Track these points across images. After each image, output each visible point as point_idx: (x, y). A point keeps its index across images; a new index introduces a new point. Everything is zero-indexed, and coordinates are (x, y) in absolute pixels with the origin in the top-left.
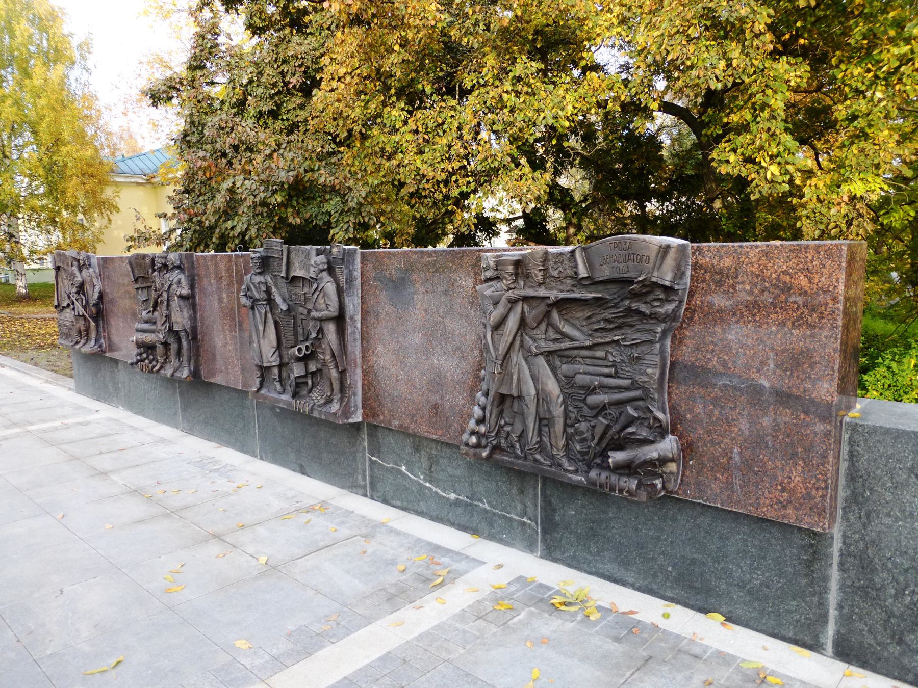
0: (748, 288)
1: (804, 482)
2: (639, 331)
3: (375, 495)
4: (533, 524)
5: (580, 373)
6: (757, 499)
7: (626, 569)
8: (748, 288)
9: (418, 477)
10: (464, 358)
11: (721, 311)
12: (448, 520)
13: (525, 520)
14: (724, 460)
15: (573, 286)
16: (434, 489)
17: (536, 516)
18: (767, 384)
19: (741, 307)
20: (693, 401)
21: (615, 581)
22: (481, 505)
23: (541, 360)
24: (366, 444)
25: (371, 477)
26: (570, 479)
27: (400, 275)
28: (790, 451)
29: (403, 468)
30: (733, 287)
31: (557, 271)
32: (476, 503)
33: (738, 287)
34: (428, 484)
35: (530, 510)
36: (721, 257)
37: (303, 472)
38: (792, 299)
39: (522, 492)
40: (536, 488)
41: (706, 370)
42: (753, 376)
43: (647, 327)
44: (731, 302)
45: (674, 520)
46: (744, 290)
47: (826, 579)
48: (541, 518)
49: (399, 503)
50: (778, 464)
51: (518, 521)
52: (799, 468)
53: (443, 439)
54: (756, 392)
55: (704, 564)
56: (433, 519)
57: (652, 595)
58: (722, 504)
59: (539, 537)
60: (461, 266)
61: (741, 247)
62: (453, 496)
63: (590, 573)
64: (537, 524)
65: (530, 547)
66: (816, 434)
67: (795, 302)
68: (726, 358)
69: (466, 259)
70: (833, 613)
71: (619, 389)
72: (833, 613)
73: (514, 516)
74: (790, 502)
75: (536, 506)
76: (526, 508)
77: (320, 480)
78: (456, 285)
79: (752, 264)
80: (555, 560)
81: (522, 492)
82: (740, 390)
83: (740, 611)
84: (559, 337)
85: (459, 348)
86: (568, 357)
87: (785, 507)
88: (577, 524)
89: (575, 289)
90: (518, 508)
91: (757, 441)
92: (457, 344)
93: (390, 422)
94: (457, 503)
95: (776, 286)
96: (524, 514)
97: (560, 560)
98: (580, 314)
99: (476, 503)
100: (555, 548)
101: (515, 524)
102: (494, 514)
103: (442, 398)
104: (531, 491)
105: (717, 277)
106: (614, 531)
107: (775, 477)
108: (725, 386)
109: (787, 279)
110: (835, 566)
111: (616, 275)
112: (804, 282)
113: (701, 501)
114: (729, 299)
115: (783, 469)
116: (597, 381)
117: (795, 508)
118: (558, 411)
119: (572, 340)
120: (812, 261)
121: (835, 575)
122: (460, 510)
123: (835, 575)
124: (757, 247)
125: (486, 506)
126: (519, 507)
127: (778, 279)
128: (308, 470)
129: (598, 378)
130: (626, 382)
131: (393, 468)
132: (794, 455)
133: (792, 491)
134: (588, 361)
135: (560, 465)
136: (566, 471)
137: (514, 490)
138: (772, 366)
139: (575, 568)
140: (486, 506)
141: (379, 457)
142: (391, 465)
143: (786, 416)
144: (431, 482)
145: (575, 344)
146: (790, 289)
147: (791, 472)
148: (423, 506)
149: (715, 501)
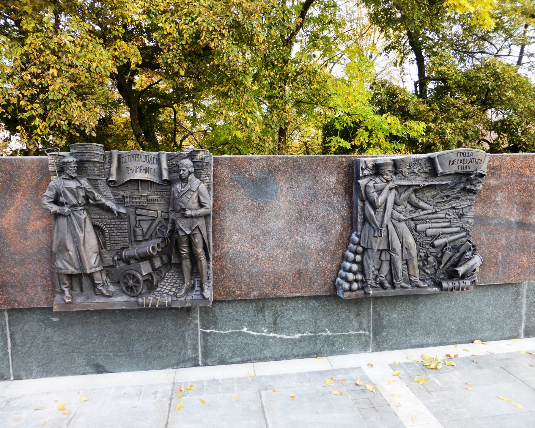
0: (506, 175)
1: (527, 261)
2: (463, 200)
3: (209, 361)
4: (367, 333)
5: (430, 228)
6: (509, 275)
7: (429, 337)
8: (506, 175)
9: (263, 332)
10: (327, 232)
11: (494, 187)
12: (292, 355)
13: (361, 332)
14: (494, 260)
15: (426, 178)
16: (278, 336)
17: (369, 327)
18: (513, 220)
19: (502, 184)
20: (481, 234)
21: (422, 346)
22: (324, 334)
23: (403, 224)
24: (198, 322)
25: (204, 347)
26: (428, 291)
27: (261, 176)
28: (522, 249)
29: (245, 330)
30: (499, 175)
31: (417, 169)
32: (320, 334)
33: (502, 175)
34: (272, 335)
35: (364, 325)
36: (494, 161)
37: (99, 369)
38: (523, 179)
39: (359, 314)
40: (369, 309)
41: (486, 217)
42: (508, 217)
43: (468, 198)
44: (498, 183)
45: (456, 300)
46: (504, 176)
47: (521, 304)
48: (373, 327)
49: (239, 359)
50: (517, 256)
51: (355, 335)
52: (526, 256)
53: (309, 294)
54: (509, 224)
55: (470, 318)
56: (276, 359)
57: (443, 345)
58: (493, 282)
59: (371, 339)
60: (326, 168)
61: (503, 156)
62: (297, 336)
63: (407, 348)
64: (369, 332)
65: (365, 347)
66: (532, 239)
67: (524, 181)
68: (496, 210)
69: (329, 163)
70: (524, 318)
71: (452, 233)
72: (524, 318)
73: (352, 333)
74: (522, 272)
75: (369, 320)
76: (356, 325)
77: (129, 370)
78: (320, 181)
79: (507, 164)
80: (383, 350)
81: (359, 314)
82: (502, 224)
83: (487, 334)
84: (413, 209)
85: (322, 226)
86: (422, 220)
87: (520, 275)
88: (398, 322)
89: (427, 180)
90: (355, 326)
91: (508, 247)
92: (321, 223)
93: (248, 294)
94: (301, 340)
95: (517, 174)
96: (360, 328)
97: (386, 348)
98: (428, 194)
99: (320, 334)
100: (383, 342)
101: (352, 338)
102: (335, 337)
103: (306, 264)
104: (365, 312)
105: (492, 171)
106: (422, 317)
107: (516, 262)
108: (495, 223)
109: (521, 170)
110: (525, 297)
111: (460, 170)
112: (528, 172)
113: (484, 284)
114: (497, 181)
115: (519, 258)
116: (440, 231)
117: (524, 274)
118: (414, 253)
119: (423, 209)
120: (531, 162)
121: (524, 300)
122: (304, 344)
123: (524, 300)
124: (510, 156)
125: (329, 333)
126: (356, 324)
127: (518, 171)
128: (107, 367)
129: (440, 229)
130: (457, 229)
131: (232, 333)
132: (524, 250)
133: (523, 267)
134: (433, 221)
135: (417, 286)
136: (424, 287)
137: (352, 315)
138: (515, 211)
139: (397, 349)
140: (329, 333)
141: (215, 328)
142: (230, 331)
143: (521, 234)
144: (275, 331)
145: (426, 212)
146: (522, 175)
147: (522, 258)
148: (266, 353)
149: (490, 282)
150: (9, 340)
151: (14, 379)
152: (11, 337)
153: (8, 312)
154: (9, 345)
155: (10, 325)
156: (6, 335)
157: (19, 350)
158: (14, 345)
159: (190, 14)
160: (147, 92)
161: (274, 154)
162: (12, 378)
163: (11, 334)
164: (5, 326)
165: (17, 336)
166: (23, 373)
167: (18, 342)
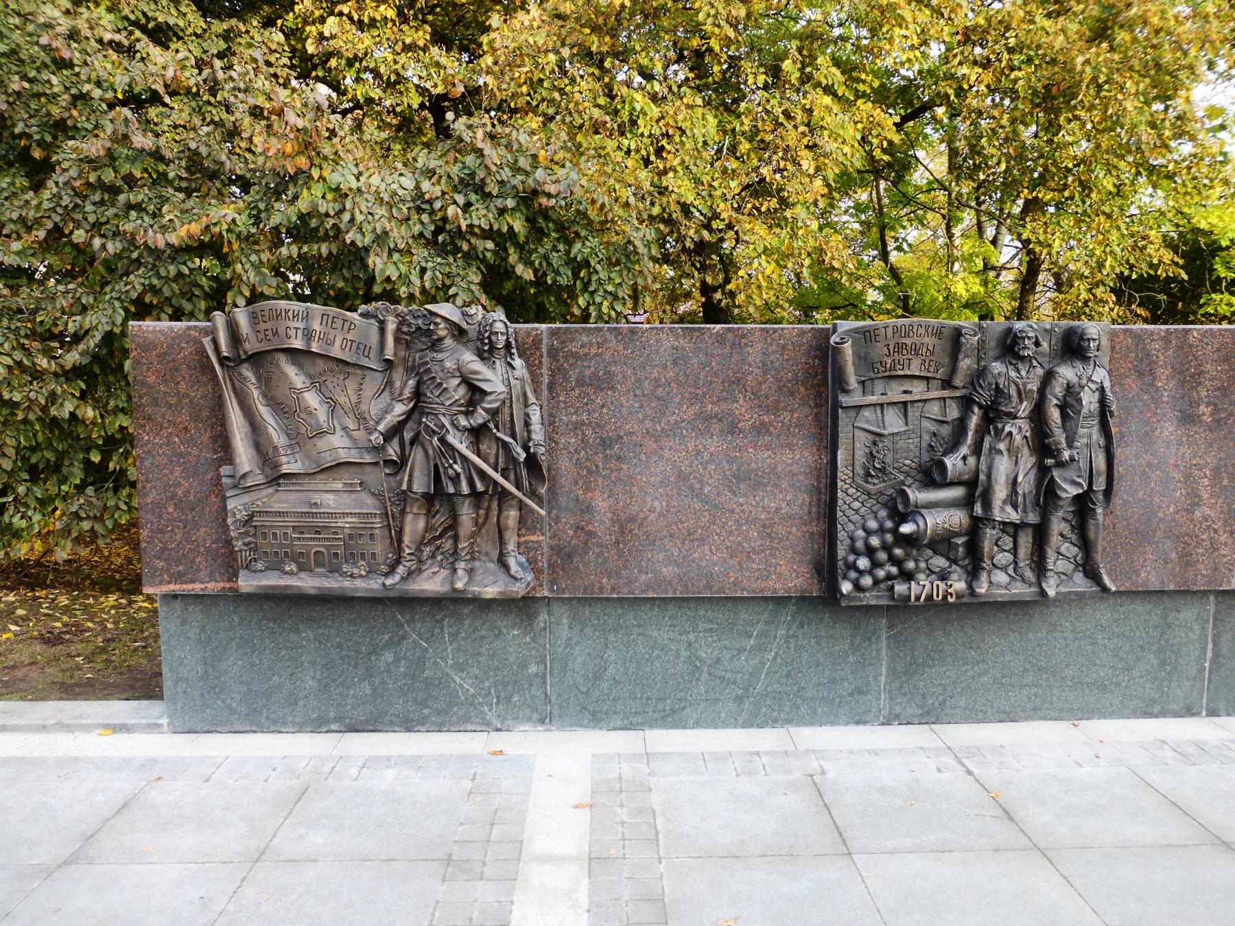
86: (551, 415)
148: (1157, 709)
150: (1210, 646)
151: (1207, 716)
152: (1214, 642)
153: (1216, 597)
154: (1209, 654)
155: (1215, 620)
156: (1206, 637)
157: (1223, 665)
158: (1216, 655)
159: (1022, 49)
160: (963, 206)
161: (177, 315)
162: (1204, 713)
163: (1214, 636)
164: (1208, 621)
165: (1226, 639)
166: (1222, 706)
167: (1224, 651)
